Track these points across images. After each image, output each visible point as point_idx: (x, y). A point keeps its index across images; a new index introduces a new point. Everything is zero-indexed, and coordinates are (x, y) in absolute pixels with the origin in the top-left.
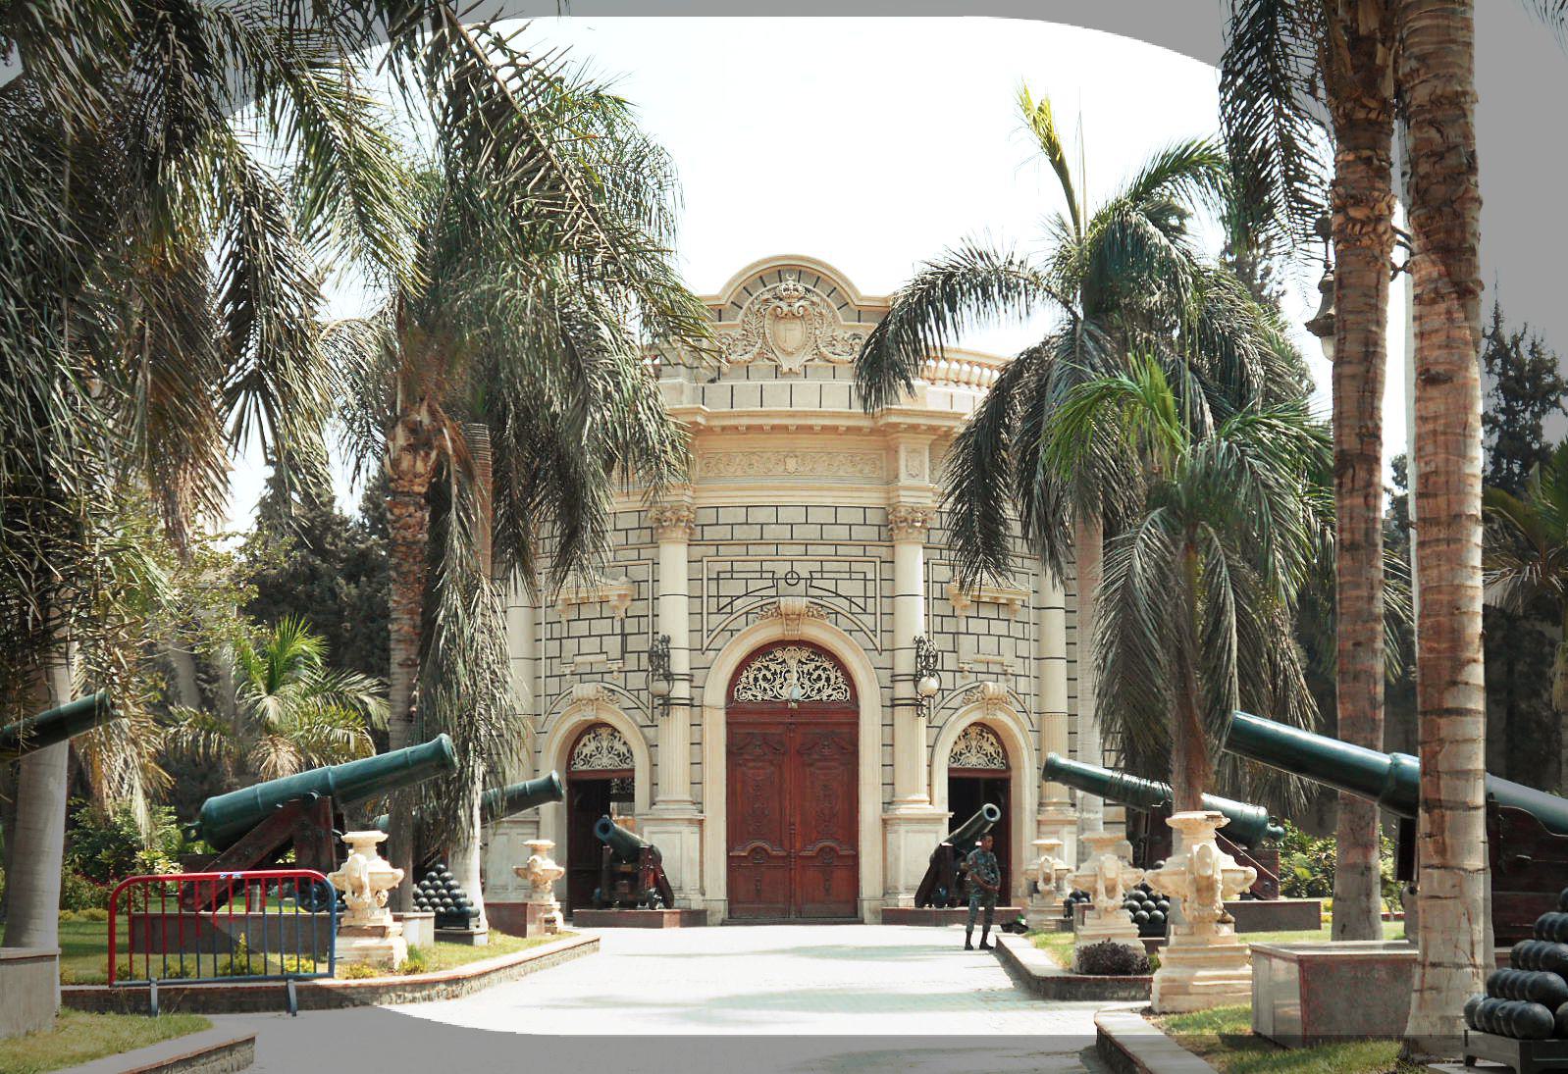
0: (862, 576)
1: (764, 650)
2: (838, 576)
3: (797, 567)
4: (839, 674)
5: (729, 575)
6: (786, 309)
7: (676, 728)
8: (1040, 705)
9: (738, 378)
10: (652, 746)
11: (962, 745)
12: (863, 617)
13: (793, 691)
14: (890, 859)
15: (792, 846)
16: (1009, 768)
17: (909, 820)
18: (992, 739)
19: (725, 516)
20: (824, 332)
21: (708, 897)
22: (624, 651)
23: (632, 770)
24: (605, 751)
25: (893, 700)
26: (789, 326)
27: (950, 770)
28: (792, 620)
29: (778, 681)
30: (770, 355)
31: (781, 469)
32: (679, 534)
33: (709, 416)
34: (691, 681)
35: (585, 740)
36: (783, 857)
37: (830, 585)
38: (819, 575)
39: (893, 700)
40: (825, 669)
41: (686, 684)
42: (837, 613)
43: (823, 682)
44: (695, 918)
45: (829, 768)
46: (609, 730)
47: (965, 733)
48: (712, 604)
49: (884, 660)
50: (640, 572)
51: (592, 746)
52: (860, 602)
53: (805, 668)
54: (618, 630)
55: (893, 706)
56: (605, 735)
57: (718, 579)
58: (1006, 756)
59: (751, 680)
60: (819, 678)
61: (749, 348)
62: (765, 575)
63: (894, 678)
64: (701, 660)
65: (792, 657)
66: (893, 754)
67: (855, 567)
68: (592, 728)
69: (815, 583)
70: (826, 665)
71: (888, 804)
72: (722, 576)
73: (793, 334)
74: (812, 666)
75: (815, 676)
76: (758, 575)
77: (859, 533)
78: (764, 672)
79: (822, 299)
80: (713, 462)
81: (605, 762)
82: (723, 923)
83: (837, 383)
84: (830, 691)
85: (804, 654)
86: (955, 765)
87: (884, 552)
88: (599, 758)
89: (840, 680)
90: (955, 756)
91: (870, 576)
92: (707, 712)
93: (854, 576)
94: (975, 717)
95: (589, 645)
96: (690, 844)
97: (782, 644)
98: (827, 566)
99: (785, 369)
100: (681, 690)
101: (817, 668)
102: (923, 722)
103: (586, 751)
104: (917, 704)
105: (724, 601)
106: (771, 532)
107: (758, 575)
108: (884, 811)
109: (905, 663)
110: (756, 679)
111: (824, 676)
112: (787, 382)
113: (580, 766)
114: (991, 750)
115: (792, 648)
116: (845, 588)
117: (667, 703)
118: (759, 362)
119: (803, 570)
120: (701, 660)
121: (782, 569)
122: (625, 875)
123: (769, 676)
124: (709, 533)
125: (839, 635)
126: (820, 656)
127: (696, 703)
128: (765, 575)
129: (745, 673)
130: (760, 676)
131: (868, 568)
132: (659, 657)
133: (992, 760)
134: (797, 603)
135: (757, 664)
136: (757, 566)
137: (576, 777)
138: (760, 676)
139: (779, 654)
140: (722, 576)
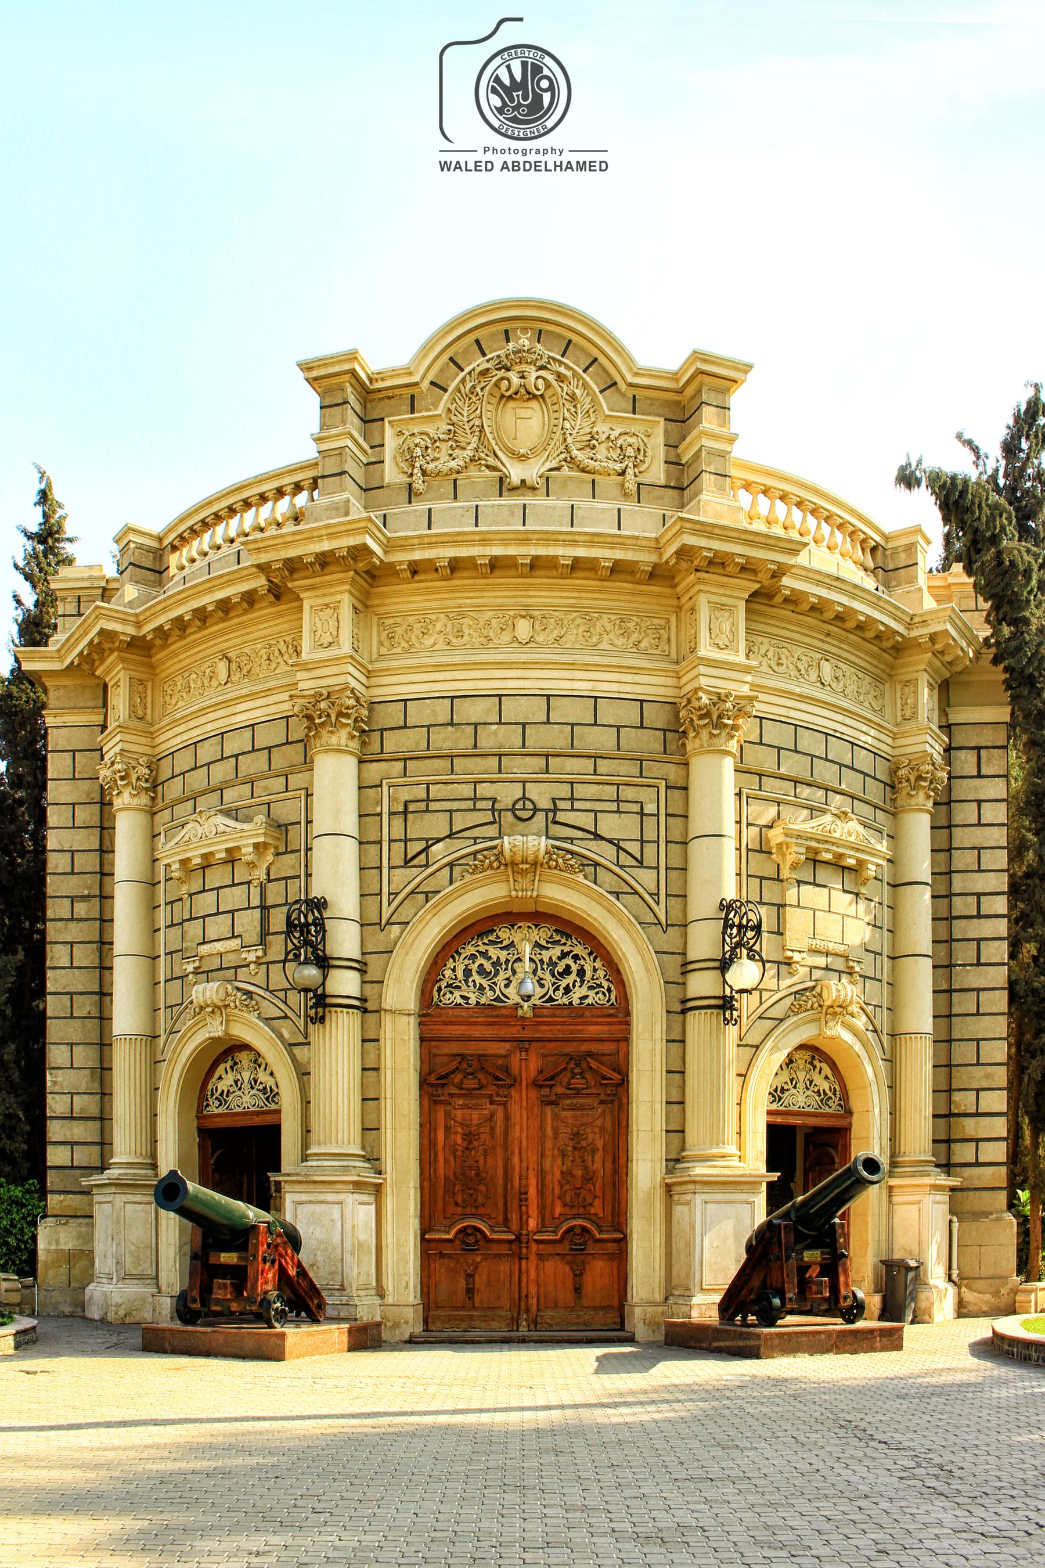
0: (636, 808)
1: (480, 927)
2: (599, 806)
3: (534, 792)
4: (598, 964)
5: (422, 806)
6: (516, 381)
7: (339, 1042)
8: (893, 1023)
9: (441, 498)
10: (303, 1074)
11: (785, 1077)
13: (525, 987)
14: (678, 1244)
15: (523, 1223)
16: (849, 1112)
17: (708, 1184)
18: (827, 1070)
19: (417, 714)
20: (579, 426)
21: (389, 1300)
22: (265, 932)
23: (278, 1112)
24: (246, 1086)
25: (684, 1001)
26: (522, 413)
28: (523, 873)
29: (502, 976)
30: (491, 461)
31: (506, 637)
32: (341, 737)
33: (389, 546)
34: (363, 972)
35: (220, 1070)
36: (510, 1242)
37: (585, 820)
38: (567, 805)
40: (576, 958)
41: (353, 977)
42: (596, 864)
43: (573, 976)
44: (366, 1338)
45: (581, 1108)
46: (252, 1056)
47: (790, 1061)
48: (389, 841)
49: (671, 939)
51: (229, 1079)
52: (634, 848)
53: (546, 955)
54: (256, 901)
55: (684, 1012)
56: (245, 1063)
58: (845, 1097)
59: (460, 975)
60: (567, 971)
61: (457, 452)
62: (480, 805)
65: (525, 940)
66: (683, 1088)
67: (628, 793)
68: (229, 1051)
69: (561, 817)
70: (579, 950)
71: (675, 1161)
72: (412, 807)
73: (527, 424)
74: (556, 952)
75: (560, 967)
76: (469, 804)
77: (631, 739)
78: (481, 960)
79: (575, 374)
80: (400, 631)
81: (247, 1101)
82: (413, 1342)
83: (599, 505)
84: (584, 991)
85: (541, 935)
87: (673, 772)
88: (237, 1096)
89: (601, 973)
90: (777, 1094)
91: (650, 808)
92: (387, 1020)
93: (624, 807)
94: (805, 1034)
95: (218, 926)
96: (357, 1223)
97: (509, 917)
98: (581, 791)
99: (515, 480)
100: (345, 983)
101: (564, 955)
102: (732, 1031)
103: (223, 1086)
105: (415, 847)
107: (469, 804)
108: (669, 1171)
109: (704, 941)
110: (467, 973)
111: (574, 968)
112: (517, 501)
113: (214, 1109)
114: (825, 1086)
116: (609, 825)
117: (321, 1004)
118: (473, 472)
119: (541, 795)
120: (378, 941)
121: (508, 794)
122: (226, 1270)
123: (488, 966)
124: (393, 742)
125: (599, 900)
126: (569, 936)
127: (369, 1006)
129: (451, 964)
131: (646, 795)
132: (305, 928)
133: (825, 1099)
134: (533, 843)
135: (470, 950)
136: (467, 791)
137: (209, 1124)
138: (474, 967)
139: (504, 934)
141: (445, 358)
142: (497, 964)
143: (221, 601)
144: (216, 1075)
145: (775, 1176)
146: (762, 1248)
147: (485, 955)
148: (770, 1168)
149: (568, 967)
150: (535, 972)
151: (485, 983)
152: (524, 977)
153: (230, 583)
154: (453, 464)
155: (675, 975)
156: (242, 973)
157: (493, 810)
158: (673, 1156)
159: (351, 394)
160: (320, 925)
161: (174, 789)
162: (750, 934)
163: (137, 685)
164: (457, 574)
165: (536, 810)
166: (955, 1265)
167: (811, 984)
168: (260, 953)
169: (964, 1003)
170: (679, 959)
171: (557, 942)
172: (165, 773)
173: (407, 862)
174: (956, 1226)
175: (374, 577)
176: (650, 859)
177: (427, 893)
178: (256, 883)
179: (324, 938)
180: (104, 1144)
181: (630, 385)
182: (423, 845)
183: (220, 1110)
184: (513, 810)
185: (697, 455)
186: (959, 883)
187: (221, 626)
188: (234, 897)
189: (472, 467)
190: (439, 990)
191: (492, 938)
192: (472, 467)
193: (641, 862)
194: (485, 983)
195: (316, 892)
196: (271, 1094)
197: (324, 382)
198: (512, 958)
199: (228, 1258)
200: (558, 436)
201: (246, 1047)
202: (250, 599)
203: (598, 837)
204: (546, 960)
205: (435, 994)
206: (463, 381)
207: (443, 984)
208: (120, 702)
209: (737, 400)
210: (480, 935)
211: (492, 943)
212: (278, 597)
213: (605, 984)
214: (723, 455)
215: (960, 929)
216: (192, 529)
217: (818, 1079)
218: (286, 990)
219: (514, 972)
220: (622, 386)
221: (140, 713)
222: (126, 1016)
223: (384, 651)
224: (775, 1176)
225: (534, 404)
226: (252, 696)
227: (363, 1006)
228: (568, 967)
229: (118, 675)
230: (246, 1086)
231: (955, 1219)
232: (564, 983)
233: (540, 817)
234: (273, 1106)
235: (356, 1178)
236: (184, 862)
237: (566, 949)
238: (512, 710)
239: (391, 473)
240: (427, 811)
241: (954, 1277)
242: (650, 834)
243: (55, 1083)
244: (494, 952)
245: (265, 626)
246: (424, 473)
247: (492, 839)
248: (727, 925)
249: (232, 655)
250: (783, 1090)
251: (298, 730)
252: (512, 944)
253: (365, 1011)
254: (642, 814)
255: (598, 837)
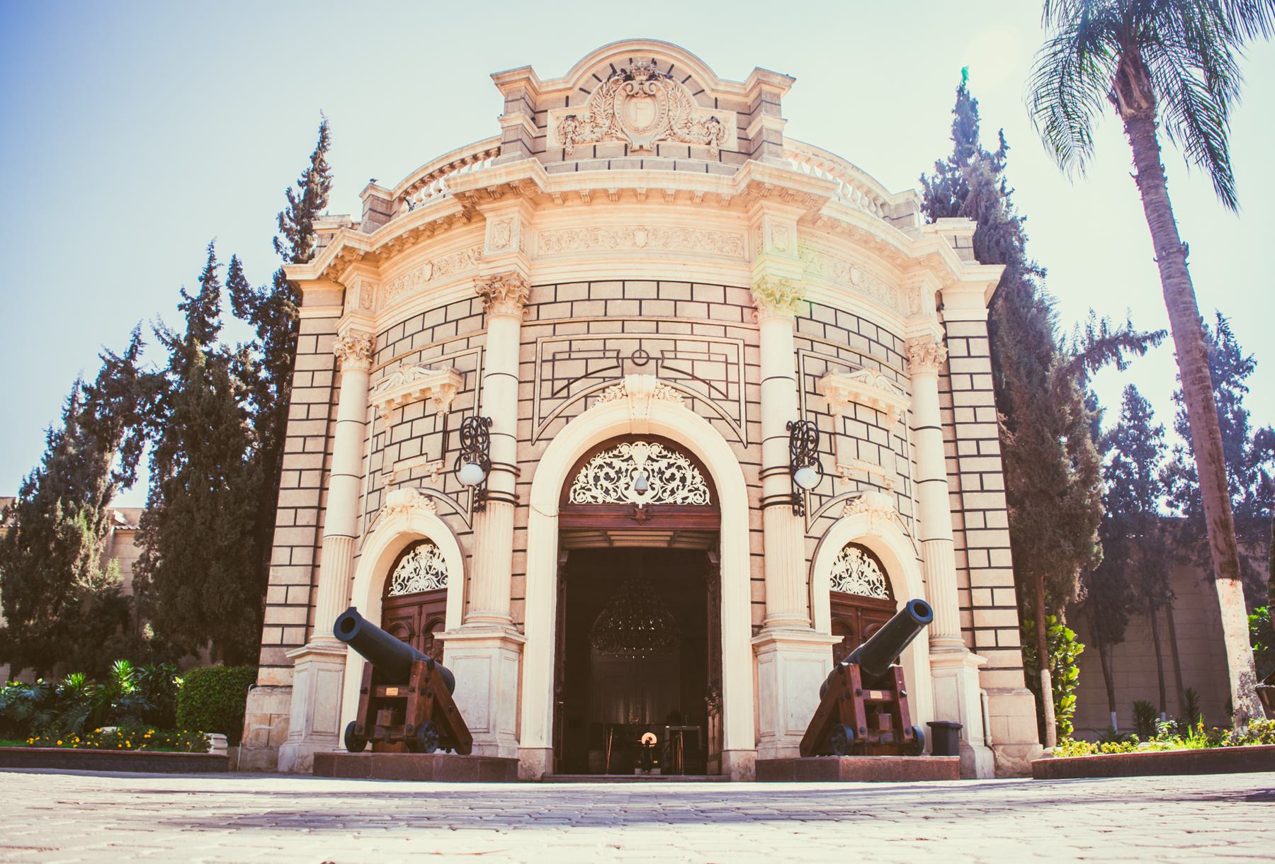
3: (647, 345)
4: (696, 472)
12: (726, 405)
18: (874, 565)
22: (445, 450)
23: (446, 590)
24: (423, 572)
27: (833, 594)
30: (619, 134)
34: (518, 476)
35: (404, 561)
37: (686, 366)
39: (762, 500)
40: (679, 468)
41: (510, 478)
42: (693, 398)
43: (677, 482)
49: (752, 454)
50: (464, 364)
53: (656, 466)
54: (440, 427)
55: (762, 508)
57: (554, 360)
58: (889, 587)
60: (673, 477)
62: (608, 354)
63: (763, 475)
64: (528, 451)
65: (640, 452)
66: (763, 567)
68: (411, 546)
69: (667, 363)
72: (558, 357)
75: (667, 475)
78: (606, 469)
81: (421, 584)
84: (685, 493)
85: (656, 449)
86: (835, 589)
90: (837, 580)
91: (732, 359)
95: (411, 448)
99: (636, 147)
100: (501, 482)
101: (670, 466)
104: (795, 500)
105: (559, 385)
106: (615, 309)
108: (754, 635)
109: (777, 453)
110: (597, 478)
111: (678, 475)
113: (396, 591)
115: (641, 443)
119: (652, 348)
121: (628, 348)
123: (613, 474)
126: (673, 452)
127: (521, 501)
128: (608, 354)
129: (584, 471)
130: (602, 475)
132: (475, 437)
135: (598, 461)
136: (599, 345)
138: (602, 475)
140: (558, 357)
141: (590, 74)
142: (619, 472)
143: (430, 223)
144: (401, 565)
145: (839, 639)
146: (835, 690)
147: (610, 465)
148: (835, 632)
149: (673, 475)
150: (648, 478)
151: (610, 486)
152: (638, 482)
153: (437, 211)
154: (594, 136)
155: (754, 480)
156: (426, 482)
157: (617, 358)
158: (757, 623)
159: (525, 97)
160: (487, 435)
161: (386, 356)
162: (811, 446)
163: (367, 287)
164: (595, 202)
165: (649, 358)
166: (988, 733)
167: (857, 494)
168: (440, 466)
169: (974, 520)
170: (757, 468)
171: (665, 457)
172: (381, 343)
173: (554, 395)
174: (986, 698)
175: (537, 204)
176: (733, 394)
177: (567, 417)
178: (440, 414)
179: (488, 447)
180: (308, 626)
181: (713, 90)
182: (566, 382)
183: (402, 593)
184: (632, 358)
185: (760, 132)
186: (962, 431)
187: (429, 241)
188: (424, 426)
189: (606, 138)
190: (575, 491)
191: (616, 452)
192: (606, 138)
193: (727, 396)
194: (610, 486)
195: (484, 414)
196: (441, 577)
197: (508, 87)
198: (630, 468)
199: (392, 692)
200: (665, 120)
201: (427, 541)
202: (450, 221)
203: (694, 378)
204: (656, 470)
205: (572, 495)
206: (601, 88)
207: (578, 487)
208: (353, 299)
209: (788, 100)
210: (607, 451)
211: (615, 456)
212: (469, 219)
213: (702, 488)
214: (779, 133)
215: (966, 465)
216: (414, 187)
217: (868, 572)
218: (458, 493)
219: (632, 478)
220: (707, 91)
221: (367, 305)
222: (337, 519)
223: (541, 253)
224: (839, 639)
225: (649, 100)
226: (447, 286)
227: (516, 501)
228: (673, 475)
229: (354, 278)
230: (423, 572)
231: (985, 693)
232: (669, 487)
233: (652, 363)
234: (443, 586)
235: (503, 635)
236: (390, 402)
237: (672, 461)
238: (633, 290)
239: (552, 142)
240: (570, 359)
241: (989, 742)
242: (733, 377)
243: (275, 577)
244: (617, 463)
245: (462, 236)
246: (573, 141)
247: (616, 378)
248: (793, 438)
249: (435, 262)
250: (841, 578)
251: (478, 306)
252: (631, 458)
253: (518, 505)
254: (727, 363)
255: (694, 378)
